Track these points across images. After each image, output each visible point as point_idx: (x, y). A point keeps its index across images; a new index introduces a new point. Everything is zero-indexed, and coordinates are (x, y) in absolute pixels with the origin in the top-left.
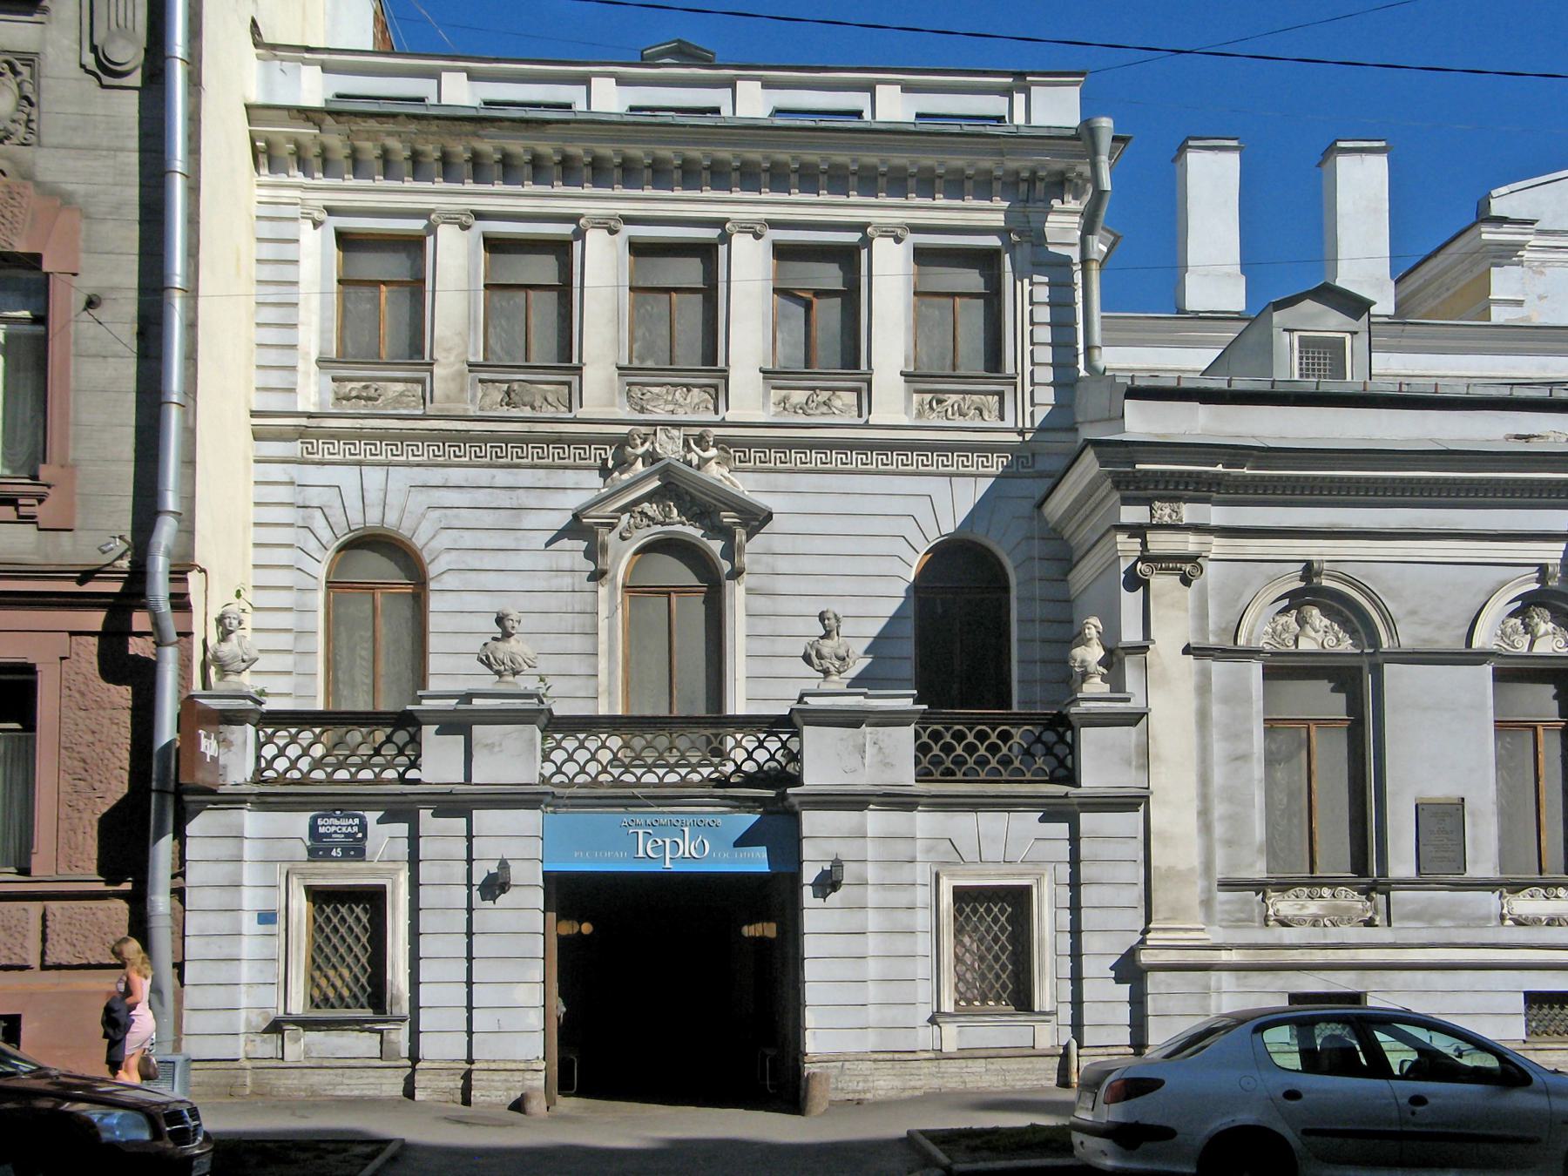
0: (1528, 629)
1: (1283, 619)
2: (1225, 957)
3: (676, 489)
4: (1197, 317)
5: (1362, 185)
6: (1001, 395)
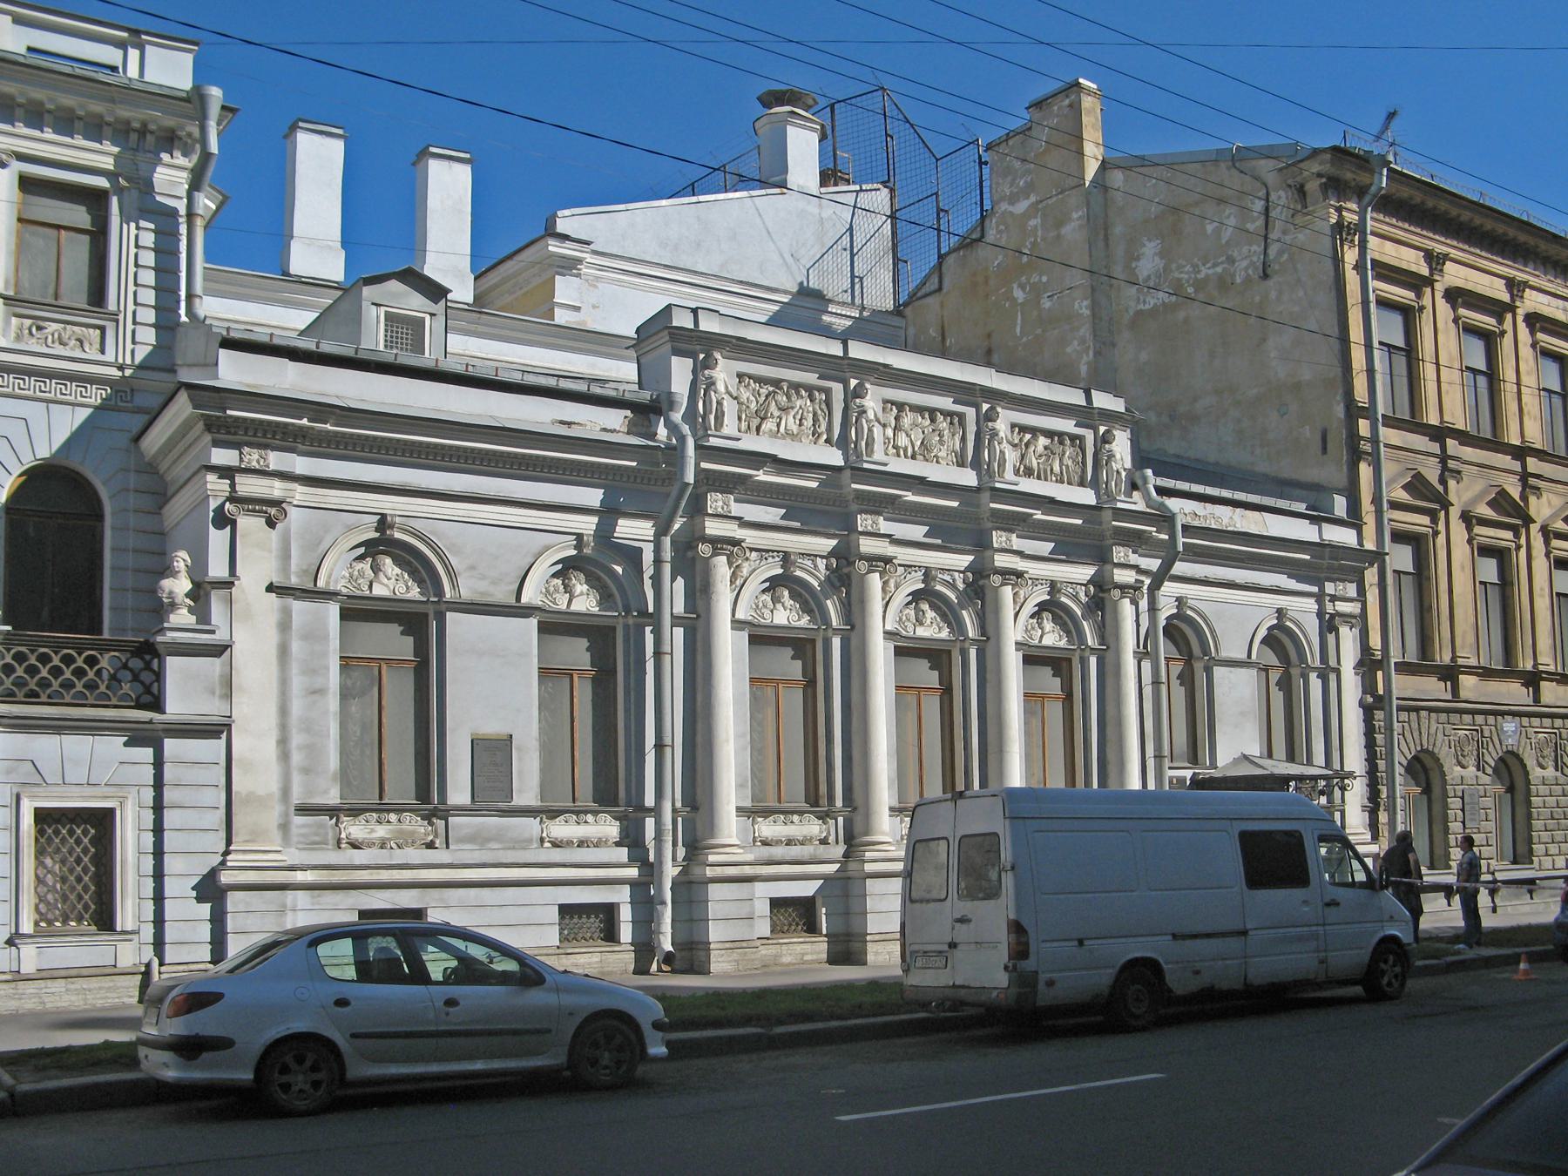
0: (568, 589)
1: (359, 566)
2: (300, 877)
4: (300, 281)
5: (449, 187)
6: (103, 329)
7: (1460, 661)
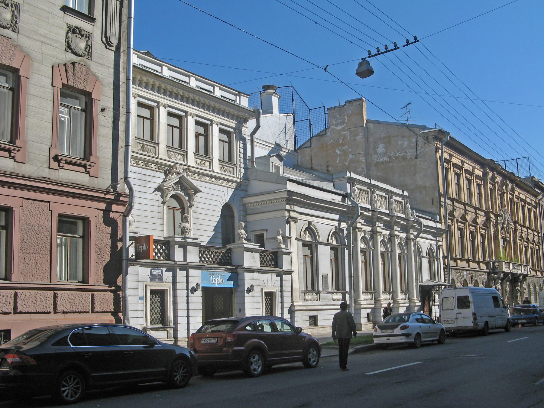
3: (182, 184)
6: (233, 168)
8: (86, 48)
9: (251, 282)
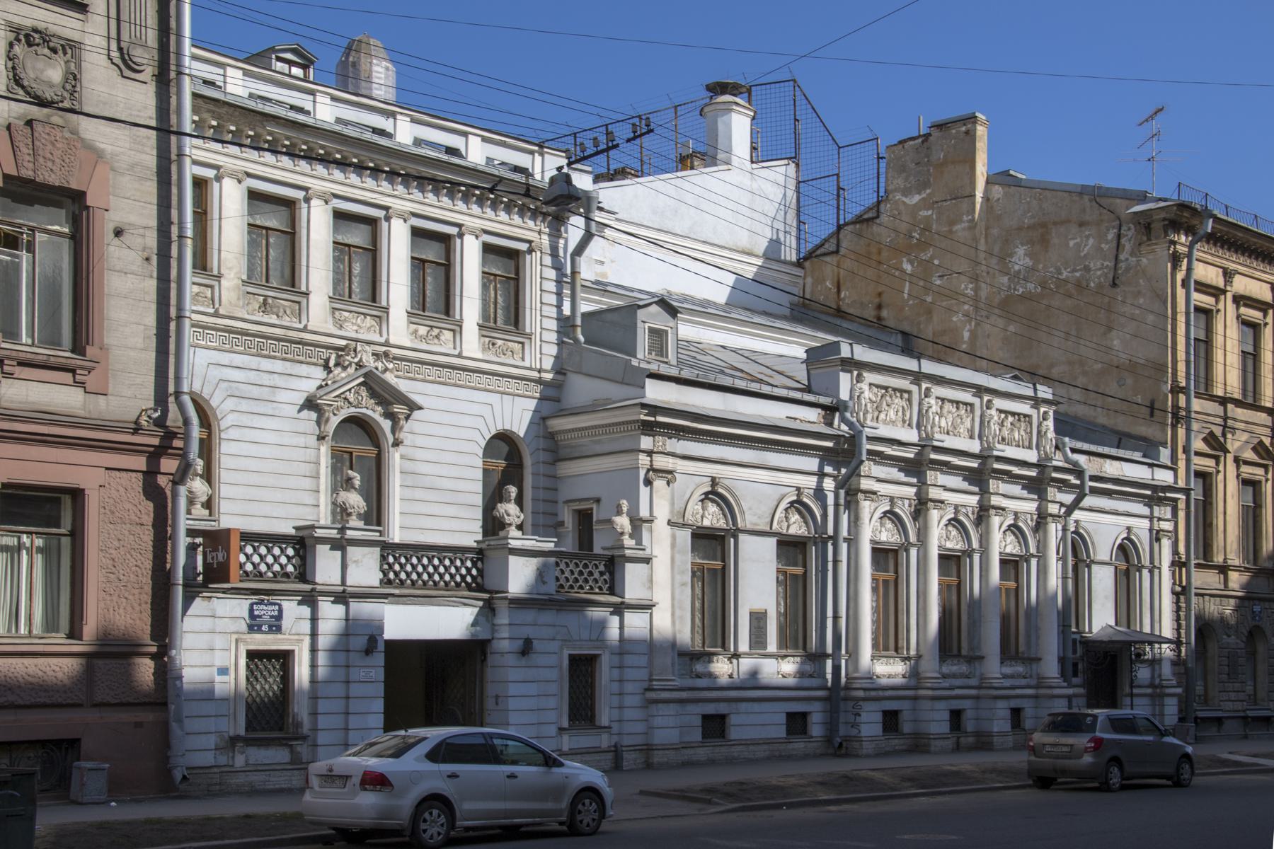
6: (523, 343)
7: (1230, 562)
8: (66, 80)
9: (369, 660)
